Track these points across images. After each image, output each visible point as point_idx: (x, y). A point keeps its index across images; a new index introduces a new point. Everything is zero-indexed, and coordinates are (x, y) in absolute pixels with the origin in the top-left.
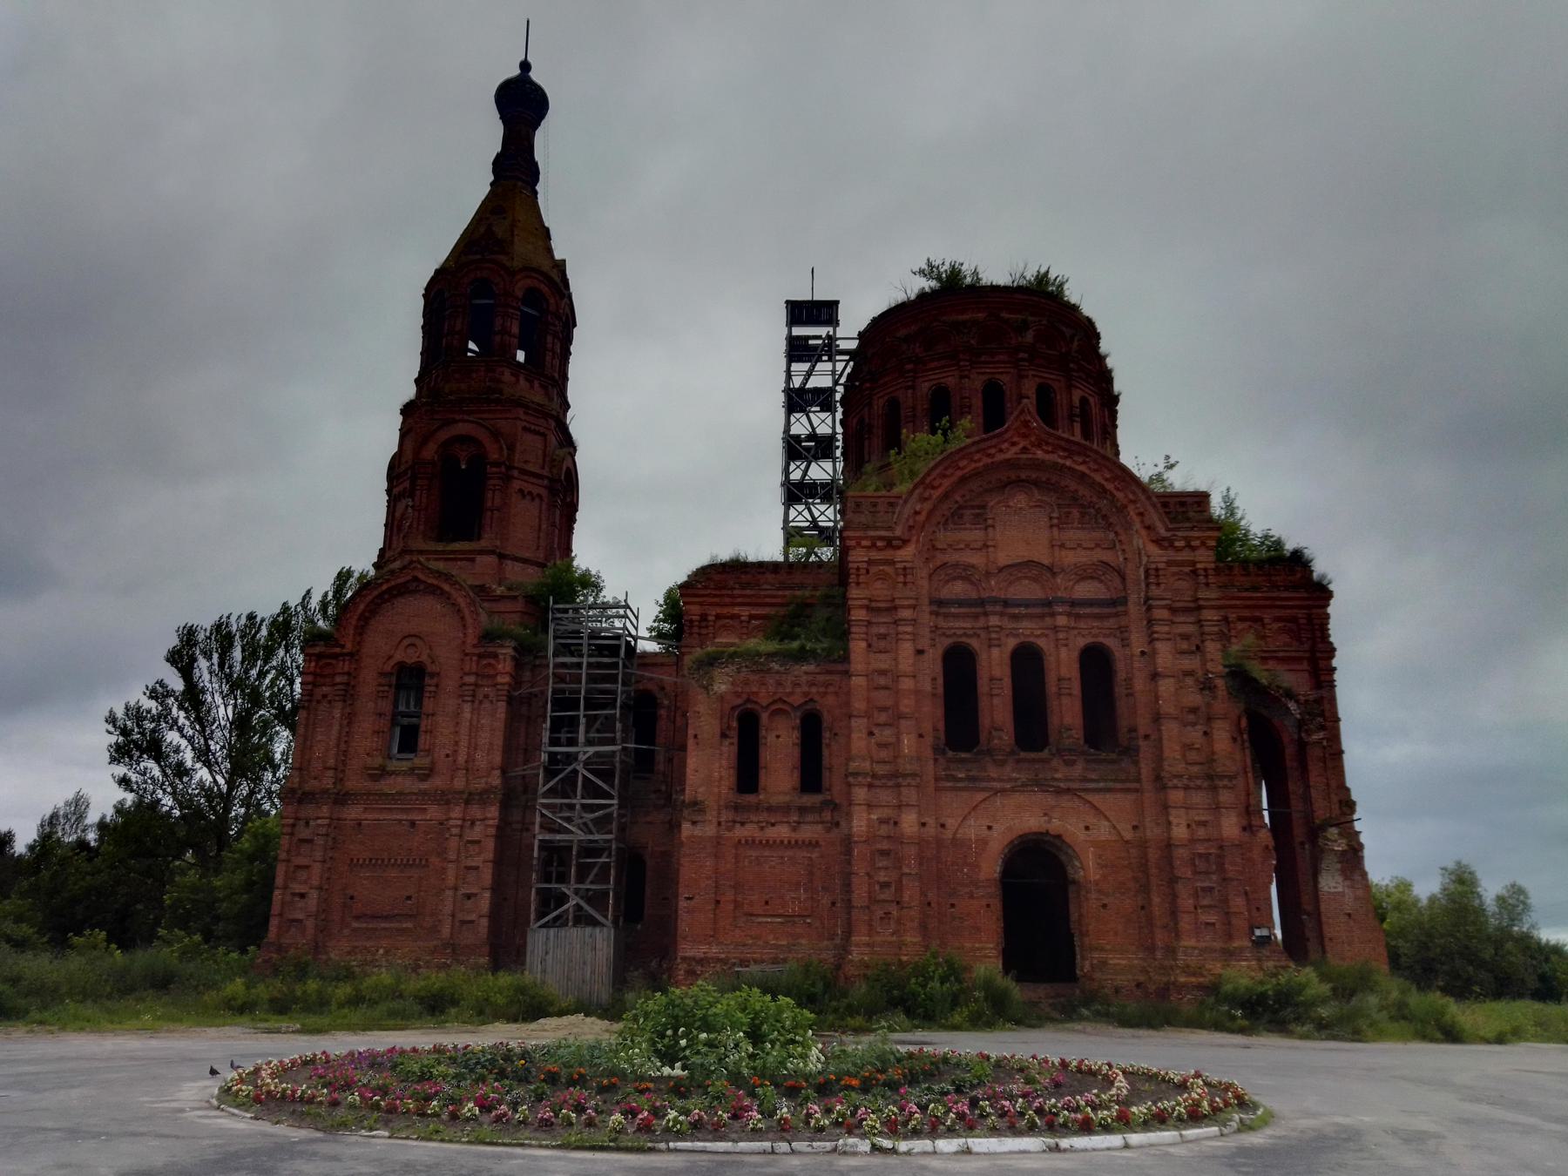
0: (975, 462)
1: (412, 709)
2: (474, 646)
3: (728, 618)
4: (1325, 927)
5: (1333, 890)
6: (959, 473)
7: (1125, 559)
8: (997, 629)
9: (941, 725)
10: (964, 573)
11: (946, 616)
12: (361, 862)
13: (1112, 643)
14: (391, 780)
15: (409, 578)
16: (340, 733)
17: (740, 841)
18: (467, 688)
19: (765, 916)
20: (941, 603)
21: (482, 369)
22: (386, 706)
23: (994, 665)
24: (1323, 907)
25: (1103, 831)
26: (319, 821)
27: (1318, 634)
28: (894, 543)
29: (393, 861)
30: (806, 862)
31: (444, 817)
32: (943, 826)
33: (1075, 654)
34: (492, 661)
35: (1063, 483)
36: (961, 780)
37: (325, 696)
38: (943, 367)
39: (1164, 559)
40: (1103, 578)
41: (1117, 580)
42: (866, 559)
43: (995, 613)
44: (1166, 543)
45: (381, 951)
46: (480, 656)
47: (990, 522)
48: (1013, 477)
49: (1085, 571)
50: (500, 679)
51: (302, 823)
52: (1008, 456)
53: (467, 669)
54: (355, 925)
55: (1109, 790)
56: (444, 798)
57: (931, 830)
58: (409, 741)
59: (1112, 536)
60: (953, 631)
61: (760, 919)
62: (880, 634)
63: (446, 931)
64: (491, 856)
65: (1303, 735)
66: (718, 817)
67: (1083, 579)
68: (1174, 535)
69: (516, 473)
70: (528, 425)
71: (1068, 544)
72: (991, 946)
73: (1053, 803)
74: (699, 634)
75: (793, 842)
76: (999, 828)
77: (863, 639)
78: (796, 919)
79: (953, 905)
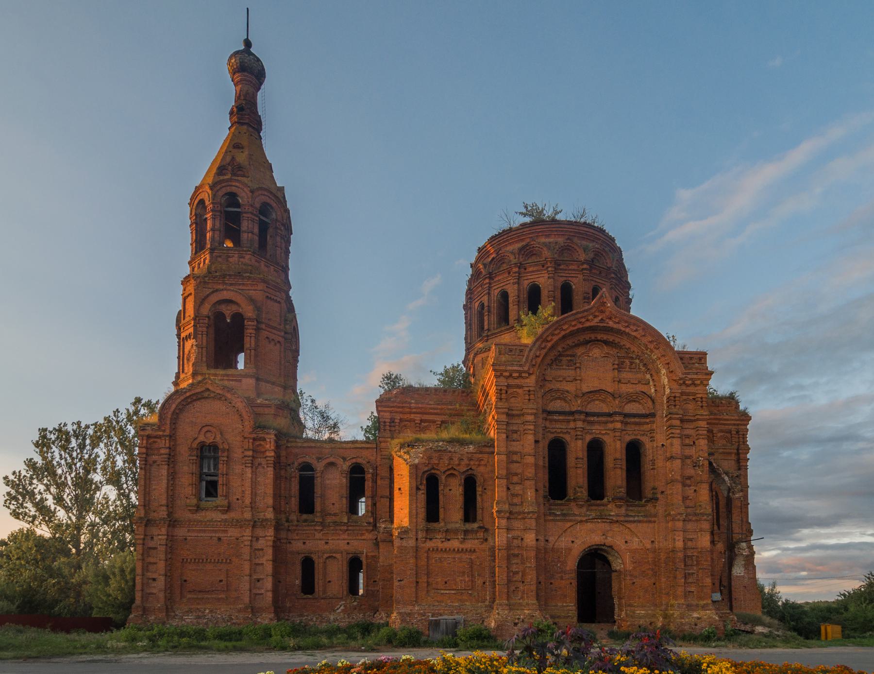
0: (564, 330)
1: (213, 471)
2: (250, 433)
3: (407, 421)
4: (733, 593)
5: (738, 575)
6: (563, 333)
7: (656, 390)
8: (582, 429)
9: (547, 485)
10: (562, 395)
11: (551, 421)
12: (189, 561)
13: (645, 439)
14: (203, 513)
15: (203, 389)
16: (168, 484)
17: (429, 549)
18: (247, 458)
19: (445, 590)
20: (550, 413)
21: (236, 255)
22: (194, 468)
23: (576, 451)
24: (733, 583)
25: (635, 543)
26: (160, 537)
27: (741, 439)
28: (523, 375)
29: (209, 560)
30: (468, 561)
31: (239, 535)
32: (547, 541)
33: (624, 445)
34: (262, 443)
35: (622, 344)
36: (559, 515)
37: (155, 462)
38: (538, 271)
39: (680, 391)
40: (641, 401)
41: (650, 403)
42: (506, 384)
43: (580, 420)
44: (681, 382)
45: (207, 611)
46: (254, 439)
47: (578, 365)
48: (593, 338)
49: (631, 397)
50: (268, 454)
51: (149, 538)
52: (592, 324)
53: (246, 447)
54: (189, 596)
55: (640, 522)
56: (239, 524)
57: (542, 543)
58: (212, 489)
59: (648, 376)
60: (554, 430)
61: (442, 592)
62: (514, 430)
63: (247, 600)
64: (271, 557)
65: (731, 494)
66: (416, 536)
67: (630, 402)
68: (686, 377)
69: (263, 326)
70: (269, 296)
71: (623, 381)
72: (572, 604)
73: (609, 528)
74: (390, 431)
75: (460, 550)
76: (578, 542)
77: (504, 433)
78: (463, 591)
79: (551, 583)
